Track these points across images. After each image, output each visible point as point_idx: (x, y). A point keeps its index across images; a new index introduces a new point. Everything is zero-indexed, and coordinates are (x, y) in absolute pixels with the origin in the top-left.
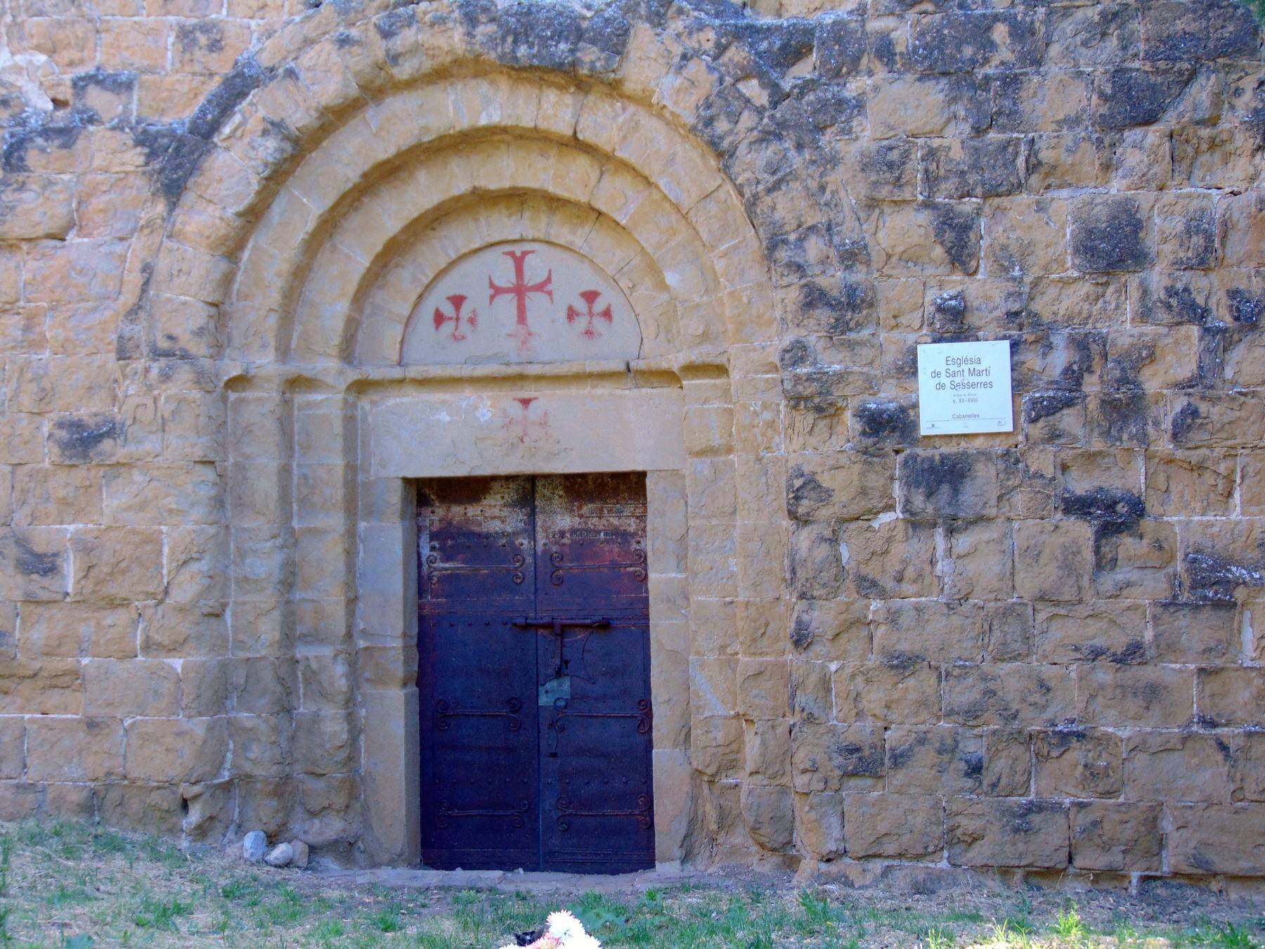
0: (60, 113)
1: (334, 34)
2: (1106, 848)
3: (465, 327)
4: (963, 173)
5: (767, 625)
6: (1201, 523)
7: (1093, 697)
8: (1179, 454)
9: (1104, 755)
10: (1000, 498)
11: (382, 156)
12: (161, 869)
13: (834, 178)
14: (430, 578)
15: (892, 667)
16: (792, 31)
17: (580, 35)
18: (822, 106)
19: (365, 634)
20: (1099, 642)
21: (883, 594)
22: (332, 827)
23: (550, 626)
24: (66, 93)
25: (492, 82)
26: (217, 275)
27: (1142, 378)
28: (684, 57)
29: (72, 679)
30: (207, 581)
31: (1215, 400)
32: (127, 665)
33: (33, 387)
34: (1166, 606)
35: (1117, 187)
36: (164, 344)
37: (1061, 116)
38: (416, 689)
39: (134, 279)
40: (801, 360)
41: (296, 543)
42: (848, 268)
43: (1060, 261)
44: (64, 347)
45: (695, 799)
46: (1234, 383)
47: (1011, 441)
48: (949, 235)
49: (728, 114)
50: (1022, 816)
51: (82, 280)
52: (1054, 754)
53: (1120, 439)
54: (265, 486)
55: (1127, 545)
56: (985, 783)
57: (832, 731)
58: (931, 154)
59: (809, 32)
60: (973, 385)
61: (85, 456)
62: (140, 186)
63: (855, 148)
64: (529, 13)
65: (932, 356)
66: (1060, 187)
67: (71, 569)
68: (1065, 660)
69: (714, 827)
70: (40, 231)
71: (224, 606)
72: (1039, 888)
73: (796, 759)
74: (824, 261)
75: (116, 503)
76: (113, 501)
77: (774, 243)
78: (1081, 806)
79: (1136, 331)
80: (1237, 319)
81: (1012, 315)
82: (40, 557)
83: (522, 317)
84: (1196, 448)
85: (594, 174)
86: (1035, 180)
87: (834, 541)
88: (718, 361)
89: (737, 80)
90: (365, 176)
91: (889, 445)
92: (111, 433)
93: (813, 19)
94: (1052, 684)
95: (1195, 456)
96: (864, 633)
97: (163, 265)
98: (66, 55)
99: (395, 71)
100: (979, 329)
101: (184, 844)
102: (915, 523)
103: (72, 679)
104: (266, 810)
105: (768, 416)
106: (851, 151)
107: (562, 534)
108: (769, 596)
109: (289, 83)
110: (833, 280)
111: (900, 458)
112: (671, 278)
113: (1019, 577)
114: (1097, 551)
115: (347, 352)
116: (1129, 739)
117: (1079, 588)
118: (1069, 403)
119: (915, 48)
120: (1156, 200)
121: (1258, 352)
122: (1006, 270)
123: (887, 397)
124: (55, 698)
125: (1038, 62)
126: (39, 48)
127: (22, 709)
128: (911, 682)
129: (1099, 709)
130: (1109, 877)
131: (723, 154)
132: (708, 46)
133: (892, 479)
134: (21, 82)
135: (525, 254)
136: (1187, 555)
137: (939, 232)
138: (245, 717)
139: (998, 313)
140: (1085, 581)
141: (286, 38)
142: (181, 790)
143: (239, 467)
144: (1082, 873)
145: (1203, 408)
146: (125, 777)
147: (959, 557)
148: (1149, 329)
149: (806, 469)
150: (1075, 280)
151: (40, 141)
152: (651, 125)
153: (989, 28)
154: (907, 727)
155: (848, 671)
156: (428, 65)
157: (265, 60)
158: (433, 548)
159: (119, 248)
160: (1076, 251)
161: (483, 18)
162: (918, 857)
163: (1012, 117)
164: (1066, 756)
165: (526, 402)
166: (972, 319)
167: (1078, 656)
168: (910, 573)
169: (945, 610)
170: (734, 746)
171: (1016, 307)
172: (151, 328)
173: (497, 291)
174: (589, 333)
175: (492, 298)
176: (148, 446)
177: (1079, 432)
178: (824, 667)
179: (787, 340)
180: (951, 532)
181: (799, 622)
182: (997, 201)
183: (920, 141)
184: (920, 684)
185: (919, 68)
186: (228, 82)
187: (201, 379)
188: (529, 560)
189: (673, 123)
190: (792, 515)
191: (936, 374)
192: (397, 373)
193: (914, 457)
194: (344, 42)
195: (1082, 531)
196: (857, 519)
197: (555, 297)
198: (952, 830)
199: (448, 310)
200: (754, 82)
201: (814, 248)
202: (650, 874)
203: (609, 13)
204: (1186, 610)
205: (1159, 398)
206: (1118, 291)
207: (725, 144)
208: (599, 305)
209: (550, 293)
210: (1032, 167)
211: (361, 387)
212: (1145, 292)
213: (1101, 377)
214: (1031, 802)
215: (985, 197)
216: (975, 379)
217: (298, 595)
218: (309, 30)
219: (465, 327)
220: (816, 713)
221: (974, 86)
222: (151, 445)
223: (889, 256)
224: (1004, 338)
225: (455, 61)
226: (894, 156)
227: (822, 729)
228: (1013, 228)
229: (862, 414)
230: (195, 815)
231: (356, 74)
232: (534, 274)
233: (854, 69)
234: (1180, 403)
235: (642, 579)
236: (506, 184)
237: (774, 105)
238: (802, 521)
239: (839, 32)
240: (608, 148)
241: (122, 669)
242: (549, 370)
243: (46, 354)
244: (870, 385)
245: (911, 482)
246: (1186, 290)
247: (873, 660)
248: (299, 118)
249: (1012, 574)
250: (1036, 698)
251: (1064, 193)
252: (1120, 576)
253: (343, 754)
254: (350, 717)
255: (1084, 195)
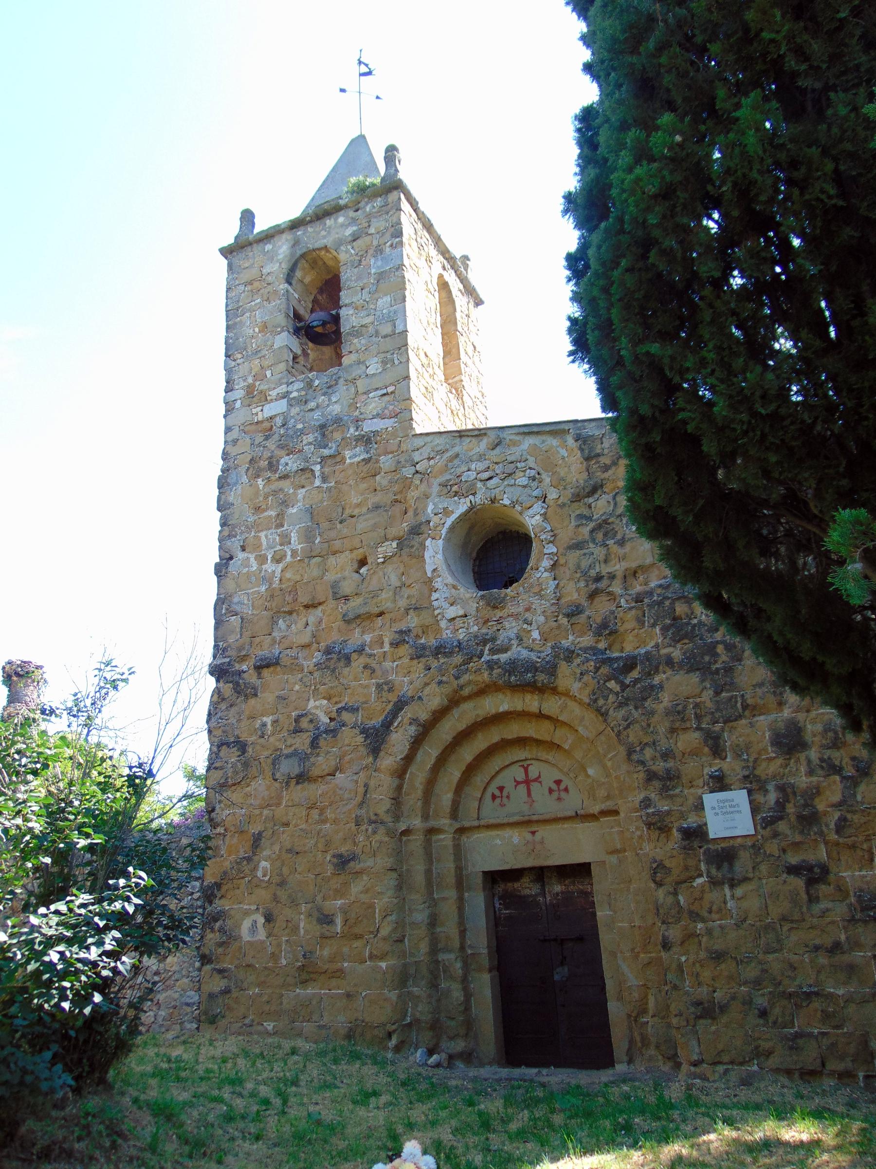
0: (332, 724)
1: (437, 680)
2: (842, 1058)
3: (505, 800)
4: (713, 713)
5: (650, 937)
6: (860, 876)
7: (819, 972)
8: (841, 840)
9: (831, 1005)
10: (754, 868)
11: (461, 729)
12: (376, 1069)
13: (654, 720)
14: (500, 918)
15: (713, 958)
16: (628, 658)
17: (536, 670)
18: (644, 689)
19: (470, 947)
20: (818, 942)
21: (703, 920)
22: (459, 1046)
23: (555, 940)
24: (334, 715)
25: (503, 693)
26: (395, 785)
27: (815, 804)
28: (581, 674)
29: (339, 974)
30: (395, 925)
31: (854, 812)
32: (363, 966)
33: (323, 840)
34: (849, 921)
35: (787, 713)
36: (373, 818)
37: (754, 683)
38: (497, 973)
39: (361, 790)
40: (648, 806)
41: (435, 905)
42: (665, 761)
43: (765, 750)
44: (335, 821)
45: (630, 1029)
46: (863, 803)
47: (754, 839)
48: (710, 742)
49: (603, 697)
50: (792, 1040)
51: (341, 792)
52: (804, 1004)
53: (809, 834)
54: (419, 878)
55: (823, 889)
56: (770, 1021)
57: (687, 993)
58: (697, 705)
59: (634, 657)
60: (732, 812)
61: (343, 869)
62: (363, 751)
63: (662, 706)
64: (514, 663)
65: (710, 800)
66: (760, 715)
67: (339, 921)
68: (801, 952)
69: (639, 1045)
70: (325, 773)
71: (404, 936)
72: (809, 1082)
73: (671, 1009)
74: (654, 759)
75: (356, 890)
76: (356, 889)
77: (630, 752)
78: (824, 1034)
79: (808, 780)
80: (857, 771)
81: (746, 777)
82: (327, 916)
83: (529, 794)
84: (850, 837)
85: (552, 728)
86: (747, 713)
87: (675, 894)
88: (614, 808)
89: (605, 682)
90: (454, 738)
91: (696, 844)
92: (353, 859)
93: (636, 652)
94: (796, 965)
95: (850, 841)
96: (696, 940)
97: (372, 783)
98: (334, 700)
99: (462, 693)
100: (731, 785)
101: (390, 1055)
102: (715, 883)
103: (339, 974)
104: (427, 1037)
105: (639, 833)
106: (661, 708)
107: (557, 894)
108: (650, 922)
109: (419, 702)
110: (660, 766)
111: (702, 851)
112: (590, 771)
113: (770, 908)
114: (808, 893)
115: (454, 814)
116: (843, 995)
117: (802, 913)
118: (781, 818)
119: (683, 659)
120: (807, 717)
121: (872, 786)
122: (740, 756)
123: (692, 821)
124: (334, 982)
125: (740, 660)
126: (324, 698)
127: (321, 989)
128: (723, 966)
129: (824, 979)
130: (846, 1076)
131: (603, 714)
132: (591, 668)
133: (700, 861)
134: (318, 712)
135: (529, 765)
136: (855, 893)
137: (706, 741)
138: (415, 990)
139: (739, 777)
140: (804, 909)
141: (418, 684)
142: (387, 1027)
143: (408, 870)
144: (832, 1073)
145: (849, 816)
146: (363, 1021)
147: (738, 899)
148: (814, 779)
149: (658, 858)
150: (774, 758)
151: (324, 735)
152: (571, 704)
153: (715, 647)
154: (725, 990)
155: (691, 961)
156: (475, 689)
157: (410, 694)
158: (500, 904)
159: (355, 777)
160: (772, 745)
161: (495, 667)
162: (741, 1064)
163: (732, 686)
164: (810, 1006)
165: (533, 833)
166: (727, 781)
167: (807, 949)
168: (715, 908)
169: (735, 927)
170: (644, 1001)
171: (747, 773)
172: (367, 812)
173: (518, 783)
174: (559, 799)
175: (516, 786)
176: (368, 864)
177: (788, 832)
178: (679, 959)
179: (642, 796)
180: (732, 886)
181: (663, 936)
182: (731, 724)
183: (691, 700)
184: (726, 967)
185: (686, 668)
186: (395, 704)
187: (390, 833)
188: (544, 908)
189: (580, 703)
190: (655, 881)
191: (714, 808)
192: (476, 823)
193: (708, 849)
194: (440, 683)
195: (798, 883)
196: (685, 882)
197: (543, 783)
198: (757, 1047)
199: (497, 793)
200: (613, 682)
201: (648, 753)
202: (610, 1071)
203: (548, 659)
204: (860, 924)
205: (825, 813)
206: (796, 762)
207: (603, 710)
208: (562, 786)
209: (540, 782)
210: (745, 707)
211: (462, 831)
212: (809, 761)
213: (794, 804)
214: (796, 1032)
215: (725, 722)
216: (733, 809)
217: (438, 930)
218: (426, 680)
219: (505, 800)
220: (678, 983)
221: (712, 673)
222: (370, 863)
223: (684, 754)
224: (744, 788)
225: (486, 686)
226: (680, 708)
227: (681, 992)
228: (740, 736)
229: (681, 830)
230: (394, 1041)
231: (446, 696)
232: (533, 774)
233: (657, 671)
234: (837, 815)
235: (594, 914)
236: (515, 736)
237: (623, 691)
238: (659, 884)
239: (648, 656)
240: (555, 717)
241: (360, 968)
242: (541, 817)
243: (328, 825)
244: (683, 816)
245: (708, 863)
246: (829, 758)
247: (703, 955)
248: (424, 716)
249: (766, 907)
250: (790, 973)
251: (762, 718)
252: (823, 905)
253: (462, 1008)
254: (465, 989)
255: (773, 717)
